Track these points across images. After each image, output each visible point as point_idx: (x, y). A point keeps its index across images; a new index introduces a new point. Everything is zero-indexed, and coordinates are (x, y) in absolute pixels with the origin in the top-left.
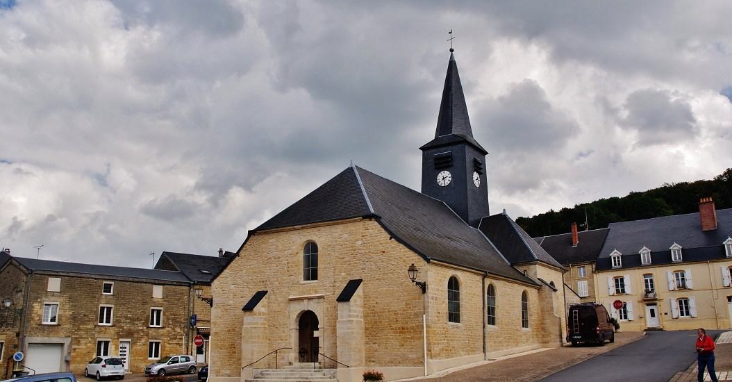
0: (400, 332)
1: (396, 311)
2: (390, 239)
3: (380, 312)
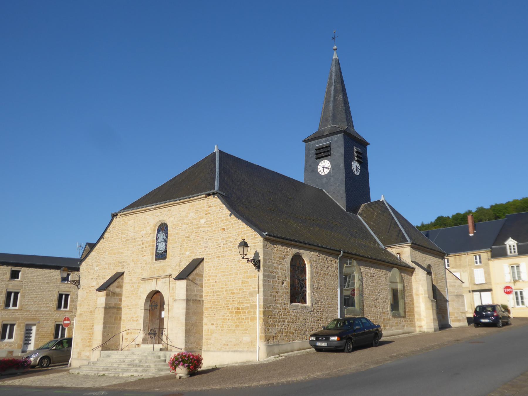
0: (236, 313)
1: (233, 290)
2: (230, 215)
3: (219, 291)
